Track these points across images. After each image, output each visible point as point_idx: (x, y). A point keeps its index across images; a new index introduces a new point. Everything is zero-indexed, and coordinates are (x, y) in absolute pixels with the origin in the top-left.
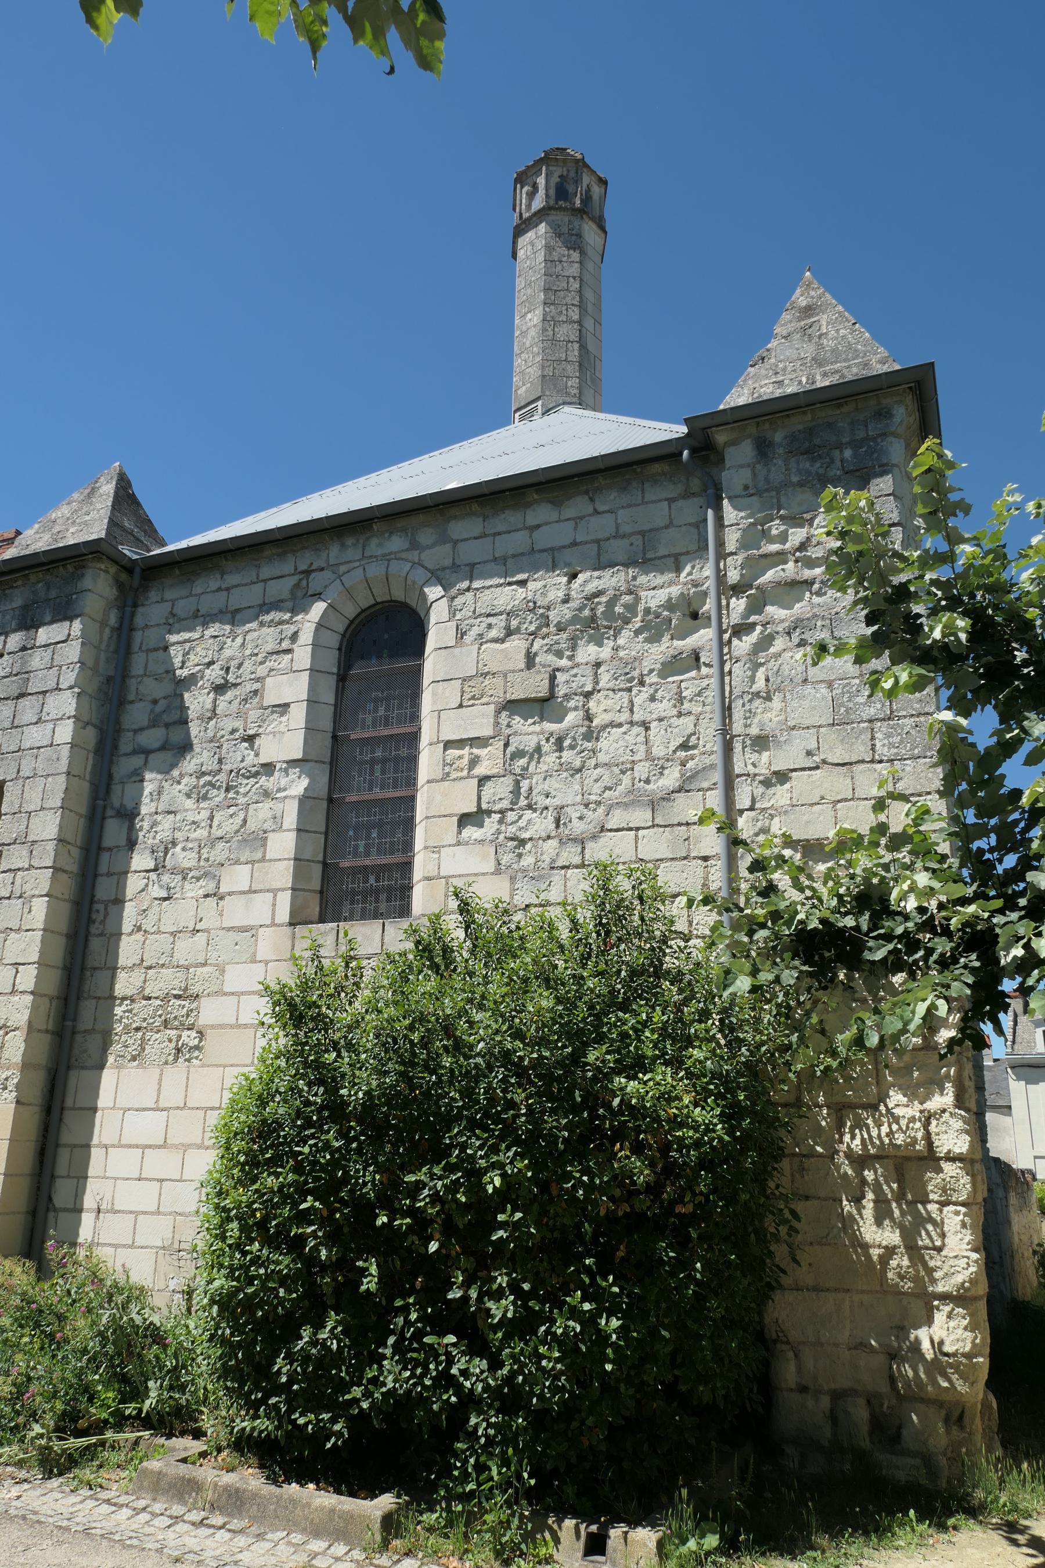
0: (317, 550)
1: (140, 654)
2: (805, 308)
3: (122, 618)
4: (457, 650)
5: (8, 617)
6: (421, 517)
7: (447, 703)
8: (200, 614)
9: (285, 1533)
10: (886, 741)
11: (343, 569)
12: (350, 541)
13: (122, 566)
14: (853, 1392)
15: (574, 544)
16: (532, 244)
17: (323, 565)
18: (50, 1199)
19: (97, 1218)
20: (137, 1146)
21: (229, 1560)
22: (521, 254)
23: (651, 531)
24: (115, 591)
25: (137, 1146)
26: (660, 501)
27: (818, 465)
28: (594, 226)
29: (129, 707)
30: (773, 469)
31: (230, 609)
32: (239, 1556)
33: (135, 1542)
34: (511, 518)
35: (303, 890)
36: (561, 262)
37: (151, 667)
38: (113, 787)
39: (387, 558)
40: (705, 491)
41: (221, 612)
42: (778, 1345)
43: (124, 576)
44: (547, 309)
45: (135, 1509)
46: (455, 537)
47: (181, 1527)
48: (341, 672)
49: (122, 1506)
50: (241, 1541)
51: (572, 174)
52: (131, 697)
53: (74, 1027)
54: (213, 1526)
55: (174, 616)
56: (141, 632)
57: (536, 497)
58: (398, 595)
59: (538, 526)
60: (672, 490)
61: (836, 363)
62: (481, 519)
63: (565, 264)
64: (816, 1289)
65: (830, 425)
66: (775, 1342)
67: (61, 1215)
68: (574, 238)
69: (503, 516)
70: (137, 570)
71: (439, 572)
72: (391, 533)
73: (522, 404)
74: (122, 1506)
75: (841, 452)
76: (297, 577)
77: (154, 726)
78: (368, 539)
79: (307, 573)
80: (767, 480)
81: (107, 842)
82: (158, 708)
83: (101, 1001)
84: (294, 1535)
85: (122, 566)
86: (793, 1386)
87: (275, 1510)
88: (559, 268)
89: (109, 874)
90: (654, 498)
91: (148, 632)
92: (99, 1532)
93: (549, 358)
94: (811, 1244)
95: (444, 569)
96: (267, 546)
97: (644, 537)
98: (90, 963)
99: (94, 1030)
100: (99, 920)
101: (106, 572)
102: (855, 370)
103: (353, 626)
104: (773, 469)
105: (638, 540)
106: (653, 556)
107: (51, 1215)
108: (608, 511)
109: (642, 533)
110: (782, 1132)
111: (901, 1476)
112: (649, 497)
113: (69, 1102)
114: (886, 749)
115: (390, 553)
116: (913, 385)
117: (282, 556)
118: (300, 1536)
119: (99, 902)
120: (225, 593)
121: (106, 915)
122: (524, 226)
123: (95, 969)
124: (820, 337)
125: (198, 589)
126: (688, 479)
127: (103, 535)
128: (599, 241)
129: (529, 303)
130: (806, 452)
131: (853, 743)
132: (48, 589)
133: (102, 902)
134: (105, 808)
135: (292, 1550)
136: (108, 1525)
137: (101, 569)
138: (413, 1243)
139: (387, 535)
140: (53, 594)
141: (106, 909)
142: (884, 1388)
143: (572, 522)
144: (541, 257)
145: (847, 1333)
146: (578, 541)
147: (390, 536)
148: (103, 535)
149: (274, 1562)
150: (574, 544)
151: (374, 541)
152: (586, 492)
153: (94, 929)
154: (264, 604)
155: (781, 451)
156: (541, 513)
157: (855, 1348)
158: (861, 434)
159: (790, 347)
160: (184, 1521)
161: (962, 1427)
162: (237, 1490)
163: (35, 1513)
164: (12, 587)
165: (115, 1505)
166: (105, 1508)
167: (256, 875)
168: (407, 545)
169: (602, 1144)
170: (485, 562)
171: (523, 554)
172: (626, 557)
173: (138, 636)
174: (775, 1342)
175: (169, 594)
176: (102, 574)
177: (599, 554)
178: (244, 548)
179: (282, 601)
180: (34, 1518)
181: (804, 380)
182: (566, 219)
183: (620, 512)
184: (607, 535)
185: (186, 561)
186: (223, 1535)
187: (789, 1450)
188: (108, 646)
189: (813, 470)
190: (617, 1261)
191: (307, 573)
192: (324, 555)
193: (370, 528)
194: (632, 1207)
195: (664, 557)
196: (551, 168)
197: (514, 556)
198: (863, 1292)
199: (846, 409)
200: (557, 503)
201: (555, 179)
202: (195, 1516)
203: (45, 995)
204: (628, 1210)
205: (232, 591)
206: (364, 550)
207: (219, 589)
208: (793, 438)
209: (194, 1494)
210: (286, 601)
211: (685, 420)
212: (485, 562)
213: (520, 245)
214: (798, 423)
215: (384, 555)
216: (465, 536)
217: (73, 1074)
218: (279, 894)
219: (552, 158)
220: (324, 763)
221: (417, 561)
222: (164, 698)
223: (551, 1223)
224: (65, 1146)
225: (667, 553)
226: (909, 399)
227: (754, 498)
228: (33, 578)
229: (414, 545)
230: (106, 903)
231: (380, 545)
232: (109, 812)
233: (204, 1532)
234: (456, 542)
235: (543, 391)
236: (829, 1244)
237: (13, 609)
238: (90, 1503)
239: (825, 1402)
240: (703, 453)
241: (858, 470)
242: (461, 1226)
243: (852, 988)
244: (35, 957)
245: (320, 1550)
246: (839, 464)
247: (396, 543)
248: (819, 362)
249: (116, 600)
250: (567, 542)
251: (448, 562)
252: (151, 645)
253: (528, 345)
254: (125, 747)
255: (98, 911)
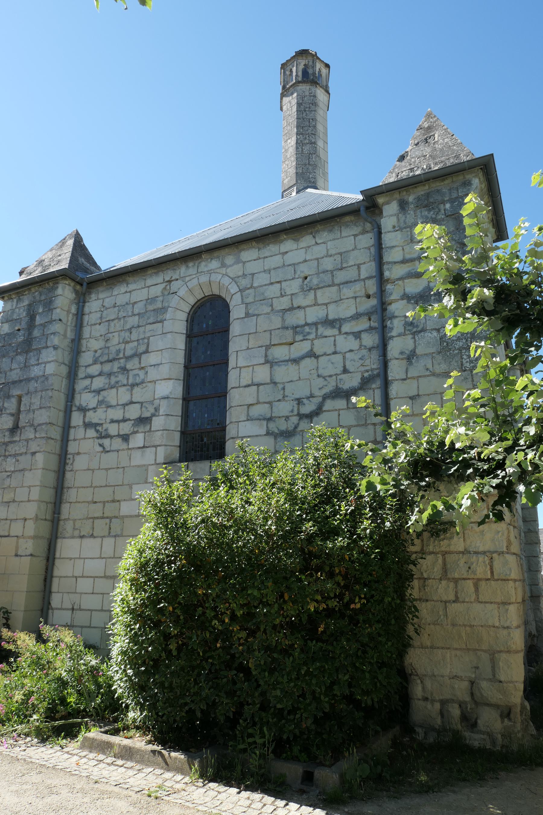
0: (174, 269)
1: (88, 327)
2: (427, 128)
3: (78, 309)
4: (246, 319)
5: (21, 310)
6: (227, 250)
7: (241, 347)
8: (116, 305)
9: (153, 769)
10: (468, 360)
11: (187, 279)
12: (191, 264)
13: (77, 282)
14: (452, 701)
15: (305, 261)
16: (290, 102)
17: (178, 277)
18: (50, 603)
19: (73, 613)
20: (91, 577)
21: (122, 782)
22: (284, 108)
23: (344, 252)
24: (74, 295)
25: (91, 577)
26: (349, 236)
27: (432, 213)
28: (323, 91)
29: (82, 354)
30: (408, 216)
31: (131, 302)
32: (128, 780)
33: (77, 772)
34: (272, 248)
35: (171, 446)
36: (305, 111)
37: (93, 333)
38: (76, 395)
39: (210, 272)
40: (373, 229)
41: (127, 304)
42: (412, 677)
43: (78, 287)
44: (298, 137)
45: (80, 757)
46: (244, 260)
47: (102, 765)
48: (188, 333)
49: (75, 755)
50: (131, 773)
51: (311, 63)
52: (84, 349)
53: (59, 517)
54: (118, 765)
55: (104, 307)
56: (87, 316)
57: (285, 237)
58: (216, 292)
59: (287, 252)
60: (356, 230)
61: (442, 157)
62: (257, 250)
63: (307, 112)
64: (432, 647)
65: (438, 191)
66: (411, 675)
67: (55, 611)
68: (312, 98)
69: (268, 248)
70: (85, 284)
71: (236, 279)
72: (212, 259)
73: (286, 188)
74: (75, 755)
75: (444, 205)
76: (165, 284)
77: (95, 364)
78: (200, 263)
79: (170, 282)
80: (405, 222)
81: (73, 423)
82: (97, 355)
83: (72, 504)
84: (157, 770)
85: (77, 282)
86: (420, 698)
87: (148, 758)
88: (305, 114)
89: (75, 440)
90: (347, 235)
91: (91, 315)
92: (60, 767)
93: (300, 163)
94: (429, 624)
95: (238, 277)
96: (149, 269)
97: (341, 255)
98: (66, 485)
99: (69, 518)
100: (70, 463)
101: (69, 285)
102: (452, 161)
103: (194, 309)
104: (408, 216)
105: (338, 257)
106: (346, 266)
107: (50, 611)
108: (323, 243)
109: (341, 254)
110: (411, 567)
111: (476, 744)
112: (344, 234)
113: (57, 555)
114: (468, 364)
115: (211, 270)
116: (482, 167)
117: (156, 273)
118: (159, 771)
119: (70, 454)
120: (129, 294)
121: (74, 460)
122: (285, 93)
123: (69, 488)
124: (434, 144)
125: (115, 292)
126: (364, 224)
127: (67, 266)
128: (326, 98)
129: (289, 134)
130: (426, 206)
131: (451, 362)
132: (41, 295)
133: (72, 454)
134: (71, 406)
135: (155, 777)
136: (66, 764)
137: (66, 284)
138: (215, 624)
139: (209, 260)
140: (43, 298)
141: (73, 457)
142: (468, 699)
143: (304, 250)
144: (295, 109)
145: (449, 671)
146: (307, 259)
147: (211, 261)
148: (67, 266)
149: (145, 783)
150: (305, 261)
151: (203, 264)
152: (311, 233)
153: (68, 468)
154: (149, 299)
155: (412, 206)
156: (288, 245)
157: (453, 678)
158: (454, 195)
159: (418, 150)
160: (104, 763)
161: (510, 719)
162: (130, 748)
163: (30, 758)
164: (23, 295)
165: (71, 754)
166: (66, 756)
167: (147, 438)
168: (220, 265)
169: (311, 573)
170: (259, 273)
171: (279, 267)
172: (332, 267)
173: (86, 318)
174: (411, 675)
175: (101, 296)
176: (67, 286)
177: (318, 266)
178: (137, 270)
179: (157, 297)
180: (29, 760)
181: (425, 167)
182: (308, 88)
183: (329, 243)
184: (322, 255)
185: (108, 278)
186: (123, 770)
187: (419, 730)
188: (71, 323)
189: (429, 215)
190: (319, 633)
191: (170, 282)
192: (178, 272)
193: (201, 257)
194: (327, 605)
195: (352, 266)
196: (299, 61)
197: (274, 269)
198: (456, 649)
199: (446, 182)
200: (296, 240)
201: (301, 67)
202: (110, 760)
203: (44, 502)
204: (325, 607)
205: (132, 293)
206: (198, 267)
207: (126, 292)
208: (418, 199)
209: (109, 749)
210: (159, 297)
211: (361, 192)
212: (259, 273)
213: (284, 103)
214: (421, 191)
215: (208, 271)
216: (249, 259)
217: (59, 541)
218: (158, 448)
219: (303, 53)
220: (180, 380)
221: (225, 273)
222: (100, 349)
223: (285, 614)
224: (56, 577)
225: (353, 264)
226: (481, 174)
227: (398, 232)
228: (33, 290)
229: (223, 265)
230: (73, 455)
231: (206, 266)
232: (74, 408)
233: (113, 768)
234: (244, 263)
235: (296, 181)
236: (439, 624)
237: (24, 306)
238: (59, 753)
239: (438, 706)
240: (372, 209)
241: (453, 215)
242: (239, 616)
243: (439, 490)
244: (38, 483)
245: (169, 778)
246: (443, 212)
247: (214, 264)
248: (432, 157)
249: (75, 299)
250: (301, 260)
251: (240, 273)
252: (93, 323)
253: (288, 157)
254: (81, 374)
255: (69, 459)
